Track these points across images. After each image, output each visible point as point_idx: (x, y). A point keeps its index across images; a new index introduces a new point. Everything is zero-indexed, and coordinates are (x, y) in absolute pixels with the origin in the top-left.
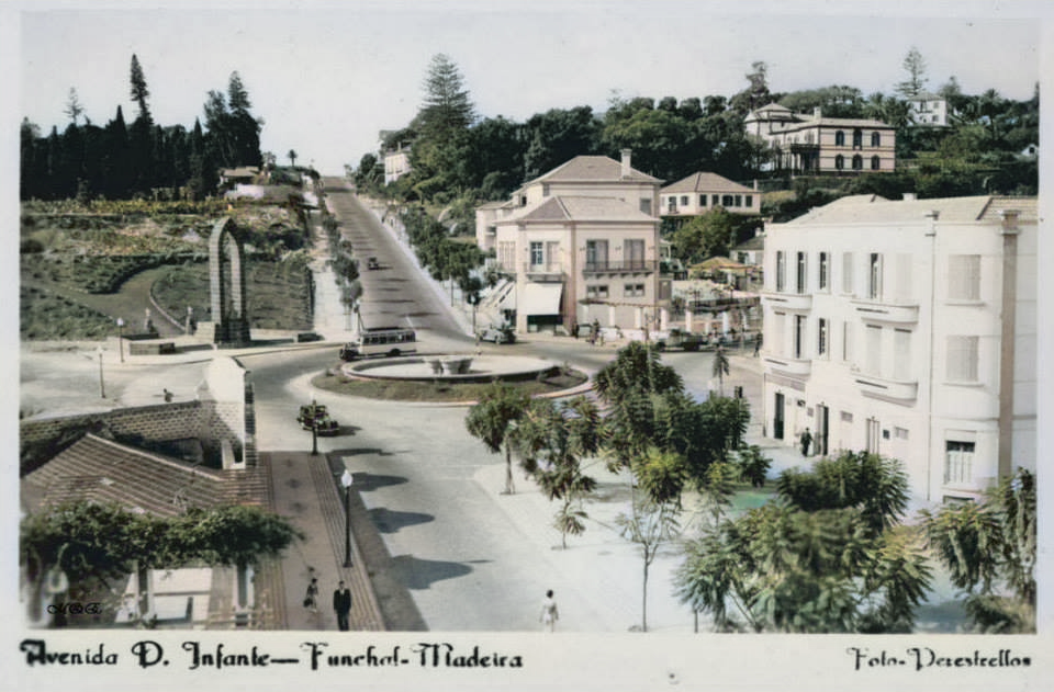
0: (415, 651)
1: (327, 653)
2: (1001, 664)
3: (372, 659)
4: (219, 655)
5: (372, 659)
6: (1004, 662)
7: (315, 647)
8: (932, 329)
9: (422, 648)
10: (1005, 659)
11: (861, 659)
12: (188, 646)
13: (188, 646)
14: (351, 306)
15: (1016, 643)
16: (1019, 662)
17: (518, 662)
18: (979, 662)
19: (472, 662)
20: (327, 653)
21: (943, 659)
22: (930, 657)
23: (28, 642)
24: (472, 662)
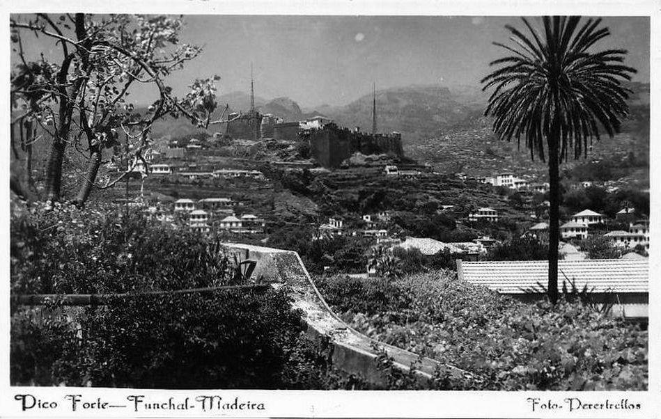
0: (199, 401)
1: (83, 400)
2: (183, 408)
3: (171, 405)
4: (549, 404)
5: (171, 405)
6: (624, 406)
7: (74, 397)
8: (532, 32)
9: (203, 398)
10: (625, 405)
11: (138, 403)
12: (130, 398)
13: (199, 399)
14: (134, 78)
15: (633, 396)
16: (633, 406)
17: (638, 406)
18: (250, 406)
19: (234, 407)
20: (83, 400)
21: (586, 405)
22: (32, 405)
23: (17, 396)
24: (234, 407)
